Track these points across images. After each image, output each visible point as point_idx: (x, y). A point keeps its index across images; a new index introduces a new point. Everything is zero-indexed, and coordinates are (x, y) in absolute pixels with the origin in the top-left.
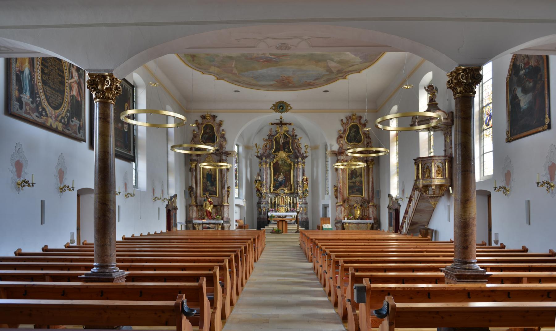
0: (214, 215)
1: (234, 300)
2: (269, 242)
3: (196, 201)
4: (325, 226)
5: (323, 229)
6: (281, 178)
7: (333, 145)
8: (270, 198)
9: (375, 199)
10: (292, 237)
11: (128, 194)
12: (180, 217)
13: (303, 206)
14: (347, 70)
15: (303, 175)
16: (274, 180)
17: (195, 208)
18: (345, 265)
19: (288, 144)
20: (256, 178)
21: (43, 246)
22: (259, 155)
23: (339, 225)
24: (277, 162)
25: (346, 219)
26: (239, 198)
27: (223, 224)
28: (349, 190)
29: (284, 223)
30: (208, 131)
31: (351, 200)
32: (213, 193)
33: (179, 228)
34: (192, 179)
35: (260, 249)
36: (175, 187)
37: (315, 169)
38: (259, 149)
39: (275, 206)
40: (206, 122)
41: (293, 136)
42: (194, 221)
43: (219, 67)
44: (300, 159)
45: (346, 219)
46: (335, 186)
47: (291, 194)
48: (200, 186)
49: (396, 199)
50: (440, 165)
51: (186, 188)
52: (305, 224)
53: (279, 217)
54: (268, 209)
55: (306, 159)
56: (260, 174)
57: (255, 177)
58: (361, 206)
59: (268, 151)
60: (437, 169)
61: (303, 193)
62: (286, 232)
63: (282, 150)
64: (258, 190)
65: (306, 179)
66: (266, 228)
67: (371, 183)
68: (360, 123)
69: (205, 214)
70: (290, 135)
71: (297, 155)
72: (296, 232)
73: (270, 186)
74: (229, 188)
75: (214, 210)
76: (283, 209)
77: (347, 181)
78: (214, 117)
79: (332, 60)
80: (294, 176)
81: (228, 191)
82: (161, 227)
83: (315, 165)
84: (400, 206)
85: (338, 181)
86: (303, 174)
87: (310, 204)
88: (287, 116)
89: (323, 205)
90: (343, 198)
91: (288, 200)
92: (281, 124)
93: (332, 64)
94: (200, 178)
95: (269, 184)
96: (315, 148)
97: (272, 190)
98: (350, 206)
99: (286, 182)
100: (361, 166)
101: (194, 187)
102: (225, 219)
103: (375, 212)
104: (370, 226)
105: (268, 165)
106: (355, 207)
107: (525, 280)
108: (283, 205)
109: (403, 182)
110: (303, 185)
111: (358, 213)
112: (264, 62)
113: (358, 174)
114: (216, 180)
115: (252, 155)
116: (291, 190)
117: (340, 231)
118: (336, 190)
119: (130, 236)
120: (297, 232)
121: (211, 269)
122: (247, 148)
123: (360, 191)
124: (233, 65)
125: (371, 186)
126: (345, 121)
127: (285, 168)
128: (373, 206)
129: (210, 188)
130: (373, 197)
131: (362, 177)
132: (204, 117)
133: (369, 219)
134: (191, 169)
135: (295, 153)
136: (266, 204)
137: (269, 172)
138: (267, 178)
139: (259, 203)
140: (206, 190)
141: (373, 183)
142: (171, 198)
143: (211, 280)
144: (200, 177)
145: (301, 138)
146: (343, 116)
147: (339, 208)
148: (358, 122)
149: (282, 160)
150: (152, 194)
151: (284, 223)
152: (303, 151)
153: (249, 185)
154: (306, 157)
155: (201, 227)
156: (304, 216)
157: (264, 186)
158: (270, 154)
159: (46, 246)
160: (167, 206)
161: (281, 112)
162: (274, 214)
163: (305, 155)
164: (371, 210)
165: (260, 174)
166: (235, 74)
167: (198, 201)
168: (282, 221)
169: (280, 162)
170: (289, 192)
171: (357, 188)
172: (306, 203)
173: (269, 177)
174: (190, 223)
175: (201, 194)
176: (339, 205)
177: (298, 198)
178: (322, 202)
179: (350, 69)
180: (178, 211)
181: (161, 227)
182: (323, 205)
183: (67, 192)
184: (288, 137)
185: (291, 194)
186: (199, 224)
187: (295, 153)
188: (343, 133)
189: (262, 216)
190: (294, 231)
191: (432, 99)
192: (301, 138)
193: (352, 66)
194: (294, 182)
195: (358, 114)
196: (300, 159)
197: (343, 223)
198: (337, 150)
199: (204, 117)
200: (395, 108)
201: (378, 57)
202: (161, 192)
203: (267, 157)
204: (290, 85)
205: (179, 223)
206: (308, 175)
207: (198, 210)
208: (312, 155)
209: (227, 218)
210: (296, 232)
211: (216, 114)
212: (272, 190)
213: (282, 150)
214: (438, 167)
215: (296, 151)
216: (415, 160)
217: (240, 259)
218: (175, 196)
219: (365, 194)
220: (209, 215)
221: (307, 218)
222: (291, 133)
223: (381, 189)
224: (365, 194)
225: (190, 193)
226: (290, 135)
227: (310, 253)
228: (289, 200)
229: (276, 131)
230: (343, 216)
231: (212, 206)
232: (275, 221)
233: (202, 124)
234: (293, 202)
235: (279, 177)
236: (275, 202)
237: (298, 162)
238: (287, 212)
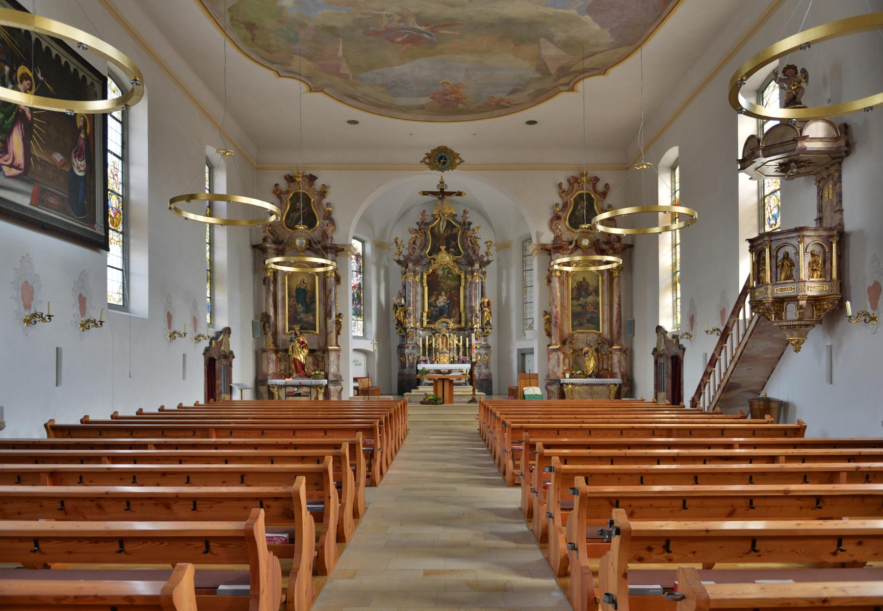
0: (309, 368)
1: (384, 472)
2: (414, 423)
3: (275, 342)
4: (530, 391)
5: (524, 397)
6: (442, 301)
7: (542, 234)
8: (421, 337)
9: (623, 337)
10: (465, 415)
11: (88, 321)
12: (242, 373)
13: (483, 351)
14: (579, 66)
15: (483, 295)
16: (430, 305)
17: (273, 356)
18: (546, 451)
19: (456, 239)
20: (396, 301)
21: (112, 413)
22: (402, 259)
23: (554, 388)
24: (434, 272)
25: (567, 375)
26: (364, 337)
27: (327, 386)
28: (573, 320)
29: (447, 384)
30: (304, 213)
31: (577, 339)
32: (308, 327)
33: (236, 397)
34: (267, 299)
35: (392, 444)
36: (229, 311)
37: (504, 286)
38: (401, 249)
39: (430, 352)
40: (294, 189)
41: (464, 224)
42: (272, 381)
43: (309, 58)
44: (477, 266)
45: (567, 375)
46: (546, 313)
47: (460, 329)
48: (284, 313)
49: (675, 337)
50: (818, 249)
51: (256, 316)
52: (485, 385)
53: (438, 372)
54: (418, 357)
55: (488, 267)
56: (403, 294)
57: (395, 300)
58: (597, 350)
59: (418, 252)
60: (809, 258)
61: (483, 329)
62: (451, 401)
63: (444, 248)
64: (400, 324)
65: (488, 303)
66: (414, 392)
67: (615, 306)
68: (595, 191)
69: (293, 366)
70: (459, 224)
71: (471, 260)
72: (470, 402)
73: (422, 316)
74: (339, 316)
75: (310, 359)
76: (445, 358)
77: (569, 303)
78: (312, 178)
79: (550, 38)
80: (465, 297)
81: (338, 323)
82: (192, 393)
83: (504, 278)
84: (684, 349)
85: (552, 302)
86: (482, 293)
87: (494, 349)
88: (453, 179)
89: (519, 350)
90: (561, 337)
91: (454, 341)
92: (442, 193)
93: (550, 51)
94: (284, 298)
95: (420, 312)
96: (504, 246)
97: (425, 323)
98: (575, 351)
99: (451, 309)
100: (609, 267)
101: (272, 314)
102: (331, 377)
103: (624, 363)
104: (614, 389)
105: (418, 278)
106: (587, 352)
107: (844, 476)
108: (445, 350)
109: (692, 300)
110: (483, 313)
111: (591, 364)
112: (404, 42)
113: (591, 289)
114: (315, 302)
115: (388, 260)
116: (460, 322)
117: (555, 401)
118: (549, 321)
119: (74, 420)
120: (473, 401)
121: (319, 460)
122: (379, 246)
123: (594, 322)
124: (340, 54)
125: (615, 312)
126: (565, 186)
127: (449, 282)
128: (620, 350)
129: (302, 316)
130: (619, 333)
131: (598, 295)
132: (290, 179)
133: (613, 375)
134: (265, 281)
135: (467, 256)
136: (413, 348)
137: (419, 289)
138: (416, 301)
139: (401, 347)
140: (298, 320)
141: (620, 306)
142: (218, 334)
143: (284, 511)
144: (283, 294)
145: (478, 228)
146: (562, 177)
147: (554, 356)
148: (591, 188)
149: (444, 269)
150: (166, 325)
151: (447, 384)
152: (482, 252)
153: (383, 315)
154: (489, 262)
155: (282, 393)
156: (484, 371)
157: (410, 315)
158: (421, 256)
159: (116, 413)
160: (207, 350)
161: (442, 170)
162: (428, 366)
163: (485, 259)
164: (615, 358)
165: (403, 294)
166: (345, 77)
167: (280, 343)
168: (443, 380)
169: (440, 272)
170: (456, 326)
171: (588, 316)
172: (488, 347)
173: (419, 299)
174: (263, 385)
175: (285, 329)
176: (554, 350)
177: (473, 335)
178: (517, 345)
179: (587, 63)
180: (235, 362)
181: (192, 393)
182: (519, 350)
183: (178, 338)
184: (455, 227)
185: (460, 329)
186: (280, 387)
187: (467, 256)
188: (562, 210)
189: (406, 371)
190: (467, 400)
191: (794, 98)
192: (478, 228)
193: (593, 55)
194: (465, 307)
195: (592, 174)
196: (477, 266)
197: (562, 385)
198: (550, 243)
199: (290, 179)
200: (673, 153)
201: (649, 31)
202: (189, 322)
203: (417, 262)
204: (460, 106)
205: (237, 385)
206: (490, 296)
207: (279, 360)
208: (499, 260)
209: (335, 375)
210: (470, 402)
211: (314, 173)
212: (425, 323)
213: (443, 251)
214: (813, 255)
215: (470, 252)
216: (750, 241)
217: (378, 435)
218: (227, 331)
219: (604, 329)
220: (300, 369)
221: (490, 375)
222: (460, 219)
223: (636, 317)
224: (604, 329)
225: (264, 325)
226: (459, 224)
227: (510, 464)
228: (456, 342)
229: (433, 216)
230: (561, 371)
231: (306, 351)
232: (430, 379)
233: (288, 192)
234: (464, 345)
235: (437, 299)
236: (430, 345)
237: (472, 272)
238: (452, 363)
